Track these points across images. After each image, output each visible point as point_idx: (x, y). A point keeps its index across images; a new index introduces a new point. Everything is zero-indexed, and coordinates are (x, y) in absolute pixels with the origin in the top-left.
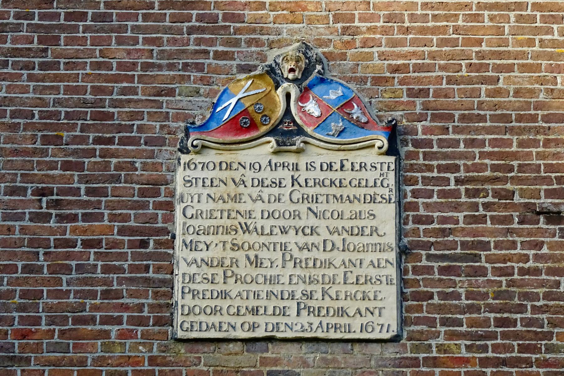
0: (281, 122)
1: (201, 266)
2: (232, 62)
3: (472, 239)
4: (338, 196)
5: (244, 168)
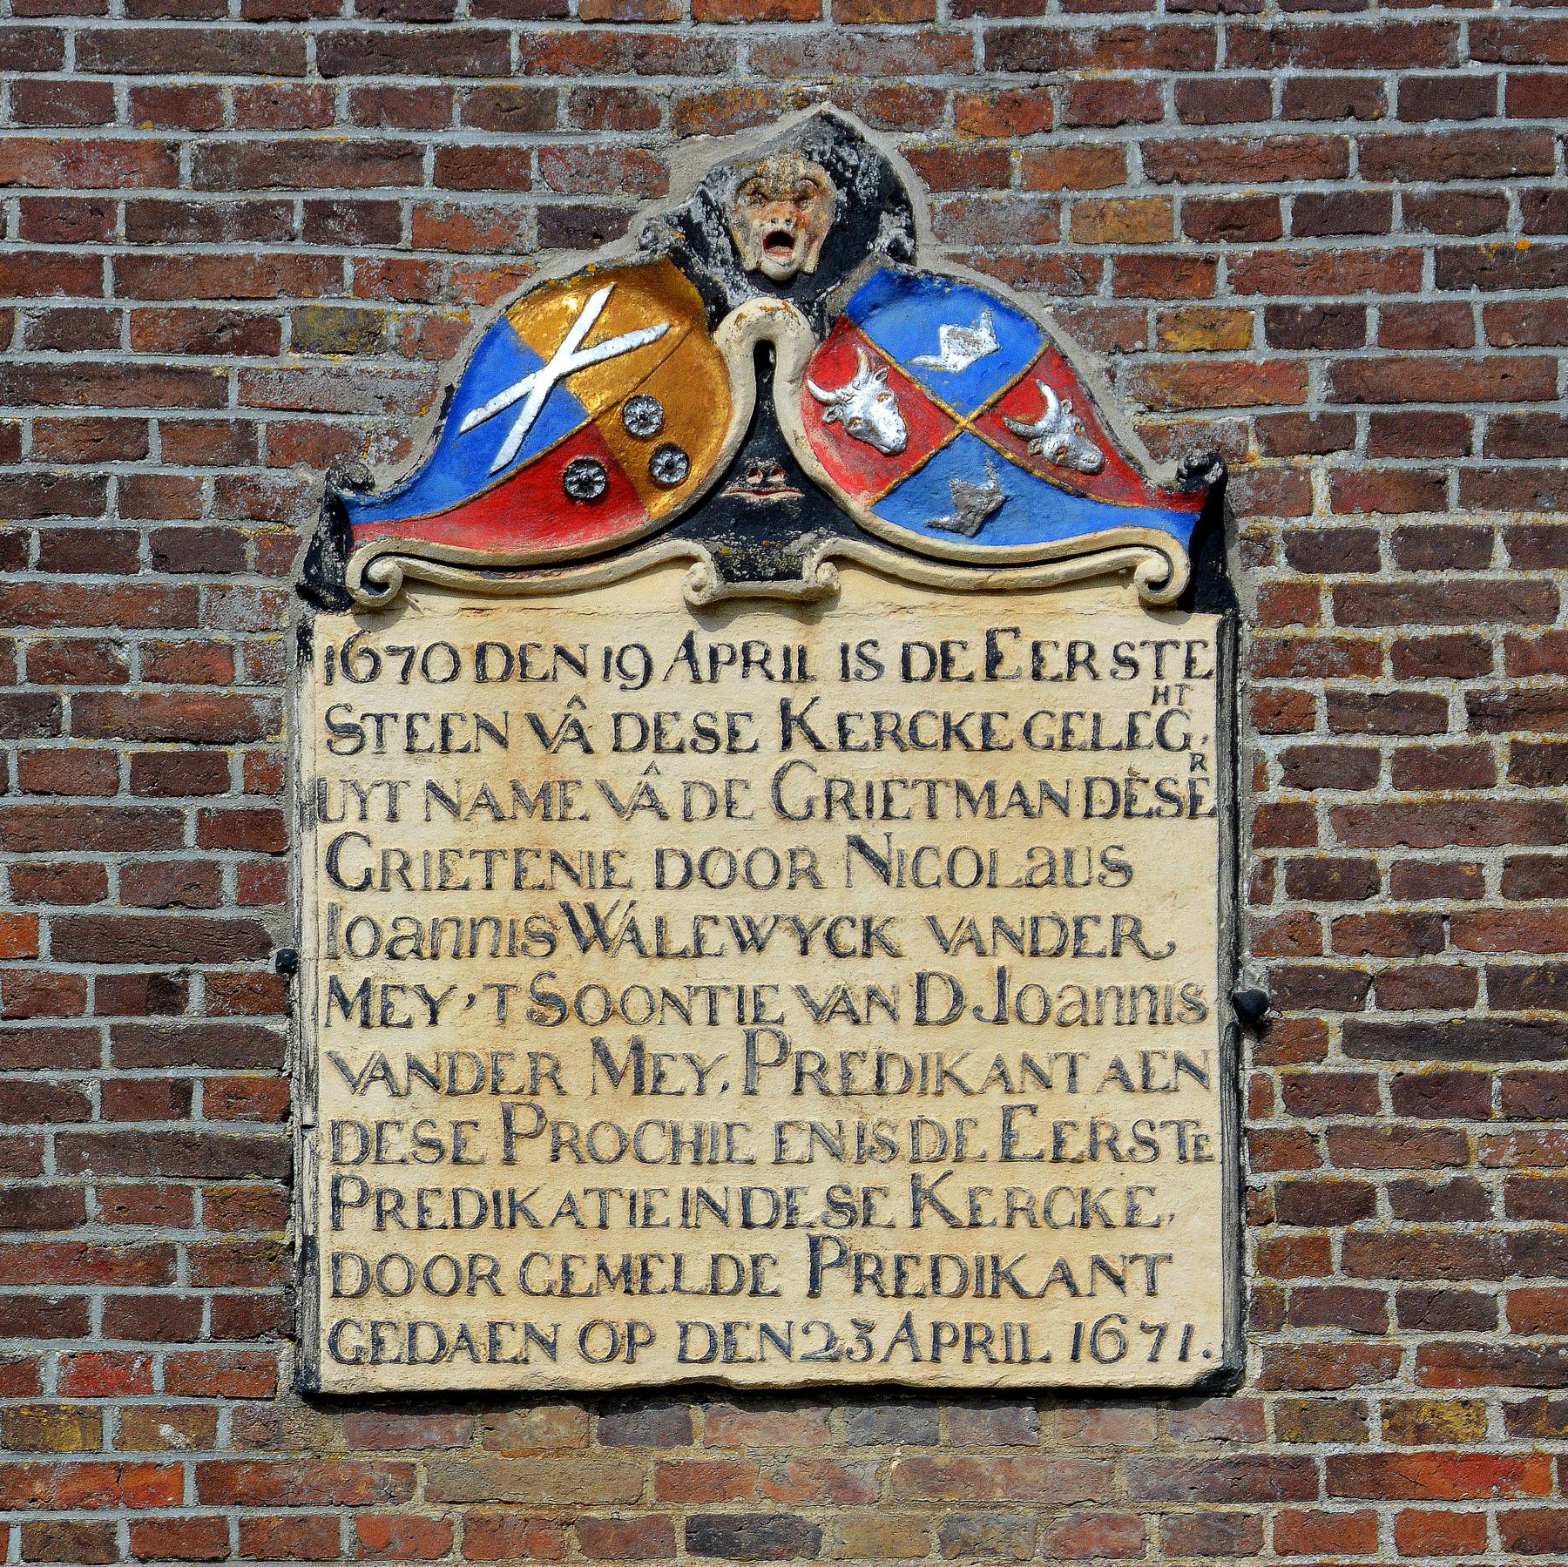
0: (734, 469)
1: (408, 1093)
2: (516, 200)
3: (1540, 961)
4: (977, 788)
5: (582, 670)
